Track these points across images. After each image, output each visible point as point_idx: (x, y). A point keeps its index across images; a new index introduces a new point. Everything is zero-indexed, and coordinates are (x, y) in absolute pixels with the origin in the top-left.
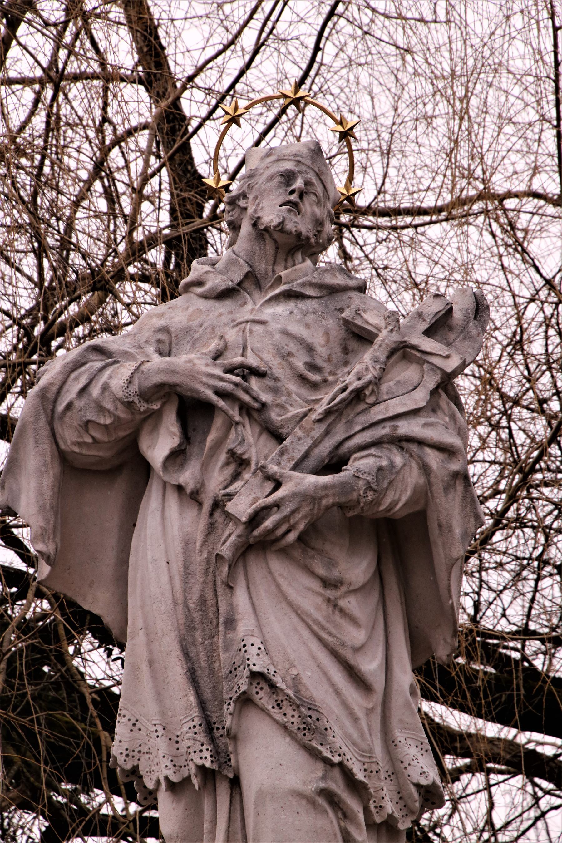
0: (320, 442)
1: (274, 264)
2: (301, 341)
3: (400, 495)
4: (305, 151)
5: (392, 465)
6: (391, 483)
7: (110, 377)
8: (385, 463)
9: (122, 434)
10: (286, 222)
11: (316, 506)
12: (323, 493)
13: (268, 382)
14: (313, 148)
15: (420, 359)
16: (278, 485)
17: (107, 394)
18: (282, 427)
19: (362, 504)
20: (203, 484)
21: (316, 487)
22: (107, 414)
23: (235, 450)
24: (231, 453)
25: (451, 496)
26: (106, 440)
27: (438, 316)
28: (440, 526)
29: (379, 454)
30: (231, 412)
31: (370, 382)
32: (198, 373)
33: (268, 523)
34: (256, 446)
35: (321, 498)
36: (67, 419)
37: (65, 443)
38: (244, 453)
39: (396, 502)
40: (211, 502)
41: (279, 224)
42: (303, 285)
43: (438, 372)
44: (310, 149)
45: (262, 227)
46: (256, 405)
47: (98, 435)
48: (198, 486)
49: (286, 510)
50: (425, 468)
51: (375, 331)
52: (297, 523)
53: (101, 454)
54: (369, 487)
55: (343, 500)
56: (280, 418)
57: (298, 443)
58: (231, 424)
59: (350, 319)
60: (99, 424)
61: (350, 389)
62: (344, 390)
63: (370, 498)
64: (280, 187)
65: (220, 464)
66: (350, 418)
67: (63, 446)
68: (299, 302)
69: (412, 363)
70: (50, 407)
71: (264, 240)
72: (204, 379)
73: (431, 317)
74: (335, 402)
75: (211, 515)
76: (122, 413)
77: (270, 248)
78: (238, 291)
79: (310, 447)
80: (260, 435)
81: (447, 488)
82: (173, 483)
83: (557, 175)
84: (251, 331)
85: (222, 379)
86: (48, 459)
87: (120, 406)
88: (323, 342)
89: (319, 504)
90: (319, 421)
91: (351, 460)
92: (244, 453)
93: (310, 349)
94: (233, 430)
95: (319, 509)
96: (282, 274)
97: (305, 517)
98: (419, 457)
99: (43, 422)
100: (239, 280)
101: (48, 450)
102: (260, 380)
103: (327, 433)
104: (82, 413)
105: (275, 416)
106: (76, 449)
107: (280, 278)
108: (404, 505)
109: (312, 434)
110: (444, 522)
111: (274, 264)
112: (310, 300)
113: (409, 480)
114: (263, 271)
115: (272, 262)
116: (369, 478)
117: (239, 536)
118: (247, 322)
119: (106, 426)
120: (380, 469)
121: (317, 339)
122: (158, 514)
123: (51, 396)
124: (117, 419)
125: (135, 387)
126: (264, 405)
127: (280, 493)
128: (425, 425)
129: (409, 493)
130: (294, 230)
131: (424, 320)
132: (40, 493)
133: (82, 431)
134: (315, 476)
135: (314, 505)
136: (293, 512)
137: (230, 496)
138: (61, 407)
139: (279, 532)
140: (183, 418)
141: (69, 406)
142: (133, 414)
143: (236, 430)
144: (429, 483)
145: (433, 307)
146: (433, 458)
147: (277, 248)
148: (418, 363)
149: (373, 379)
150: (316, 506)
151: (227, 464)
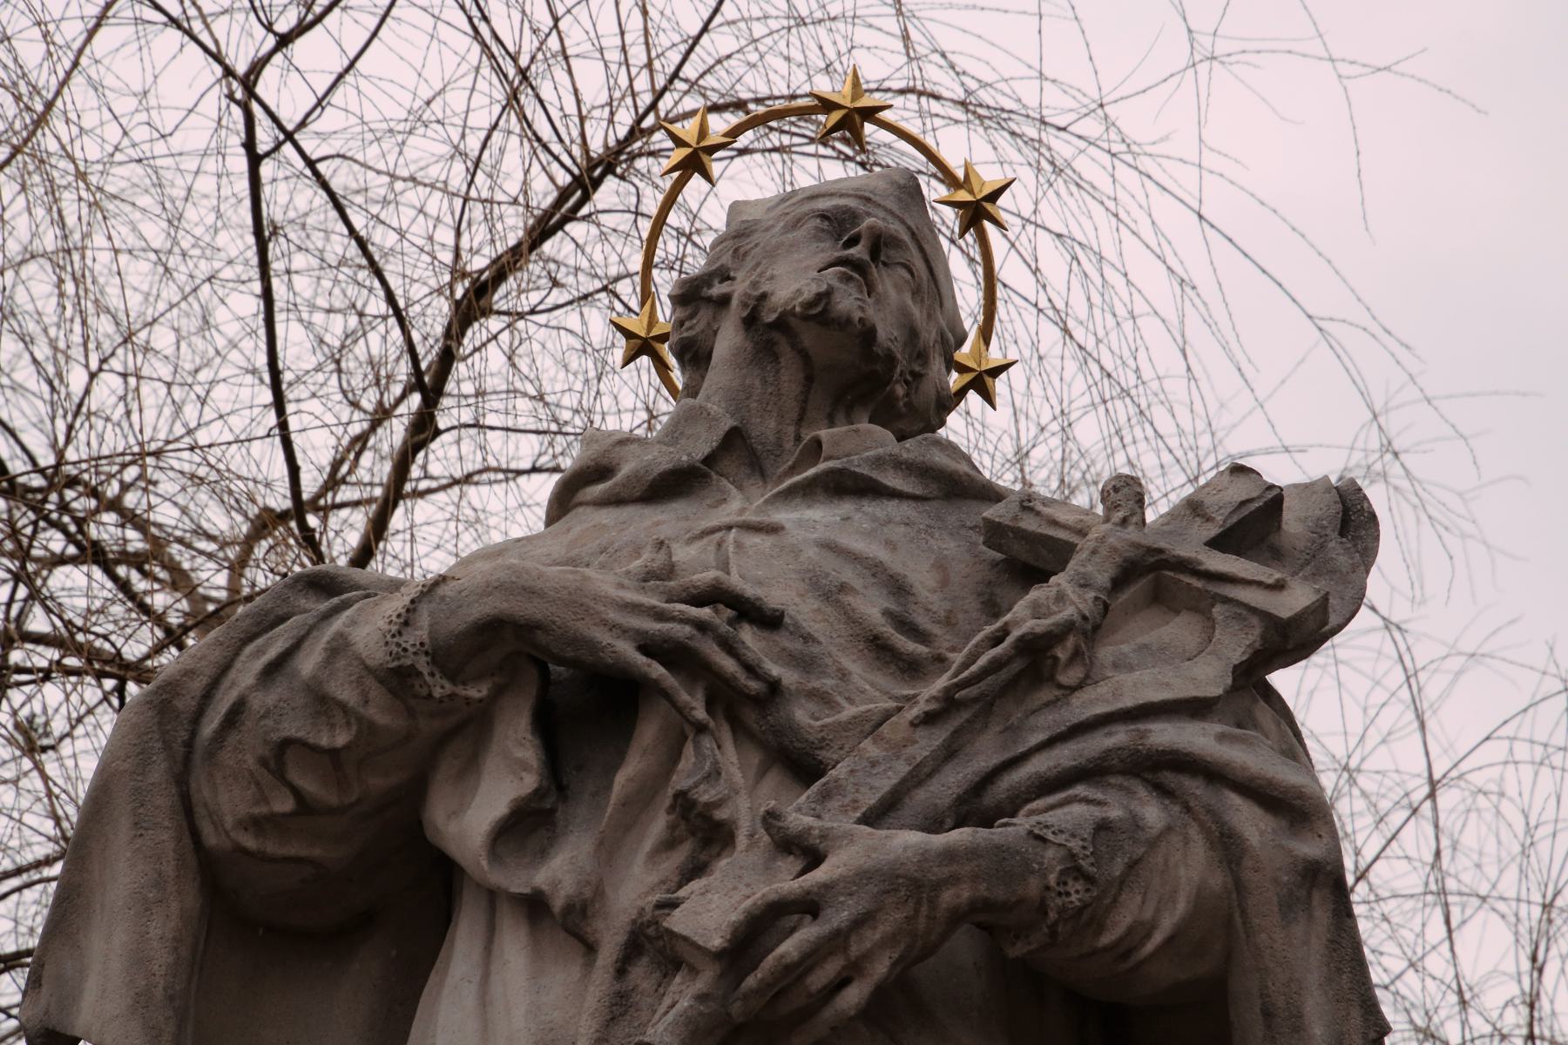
0: (930, 775)
1: (800, 420)
2: (875, 569)
3: (1158, 910)
4: (882, 185)
5: (1136, 823)
6: (1133, 865)
7: (353, 622)
8: (1115, 813)
9: (378, 783)
10: (837, 297)
11: (924, 909)
12: (946, 871)
13: (784, 640)
14: (902, 182)
15: (1202, 593)
16: (814, 858)
17: (341, 663)
18: (824, 744)
19: (1052, 915)
20: (599, 892)
21: (925, 855)
22: (339, 718)
23: (693, 795)
24: (684, 804)
25: (1298, 930)
26: (333, 799)
27: (1245, 511)
28: (1268, 1014)
29: (1099, 796)
30: (684, 696)
31: (1068, 627)
32: (596, 598)
33: (789, 948)
34: (750, 794)
35: (938, 886)
36: (227, 757)
37: (218, 824)
38: (718, 804)
39: (1141, 931)
40: (621, 938)
41: (820, 297)
42: (879, 462)
43: (1255, 621)
44: (893, 183)
45: (772, 317)
46: (754, 686)
47: (309, 785)
48: (588, 892)
49: (838, 916)
50: (1227, 845)
51: (1073, 539)
52: (867, 956)
53: (317, 852)
54: (1074, 870)
55: (1000, 893)
56: (819, 723)
57: (864, 772)
58: (683, 732)
59: (1006, 521)
60: (315, 749)
61: (1016, 633)
62: (996, 640)
63: (1074, 897)
64: (819, 240)
65: (648, 845)
66: (1014, 720)
67: (211, 838)
68: (865, 502)
69: (1177, 612)
70: (183, 735)
71: (775, 358)
72: (613, 615)
73: (1226, 512)
74: (974, 668)
75: (621, 972)
76: (380, 713)
77: (790, 377)
78: (706, 476)
79: (903, 781)
80: (762, 773)
81: (1290, 906)
82: (514, 889)
83: (1375, 979)
84: (739, 545)
85: (661, 616)
86: (169, 869)
87: (376, 691)
88: (932, 583)
89: (933, 903)
90: (929, 719)
91: (1022, 812)
92: (718, 804)
93: (898, 587)
94: (689, 749)
95: (931, 918)
96: (824, 433)
97: (889, 941)
98: (1210, 811)
99: (158, 772)
100: (707, 450)
101: (170, 846)
102: (766, 634)
103: (949, 753)
104: (269, 722)
105: (802, 715)
106: (249, 842)
107: (817, 443)
108: (1170, 941)
109: (910, 750)
110: (1280, 1002)
111: (800, 420)
112: (895, 502)
113: (1182, 871)
114: (772, 438)
115: (795, 415)
116: (1075, 844)
117: (702, 998)
118: (729, 528)
119: (333, 753)
120: (1103, 827)
121: (921, 577)
122: (469, 995)
123: (186, 703)
124: (368, 729)
125: (420, 633)
126: (774, 687)
127: (820, 874)
128: (1221, 738)
129: (1182, 907)
130: (857, 315)
131: (1209, 519)
132: (138, 959)
133: (266, 778)
134: (920, 834)
135: (919, 903)
136: (859, 923)
137: (673, 905)
138: (209, 727)
139: (819, 979)
140: (547, 726)
141: (237, 712)
142: (411, 713)
143: (697, 747)
144: (1239, 887)
145: (1230, 492)
146: (1248, 820)
147: (809, 379)
148: (1195, 609)
149: (1076, 617)
150: (924, 909)
151: (669, 844)
